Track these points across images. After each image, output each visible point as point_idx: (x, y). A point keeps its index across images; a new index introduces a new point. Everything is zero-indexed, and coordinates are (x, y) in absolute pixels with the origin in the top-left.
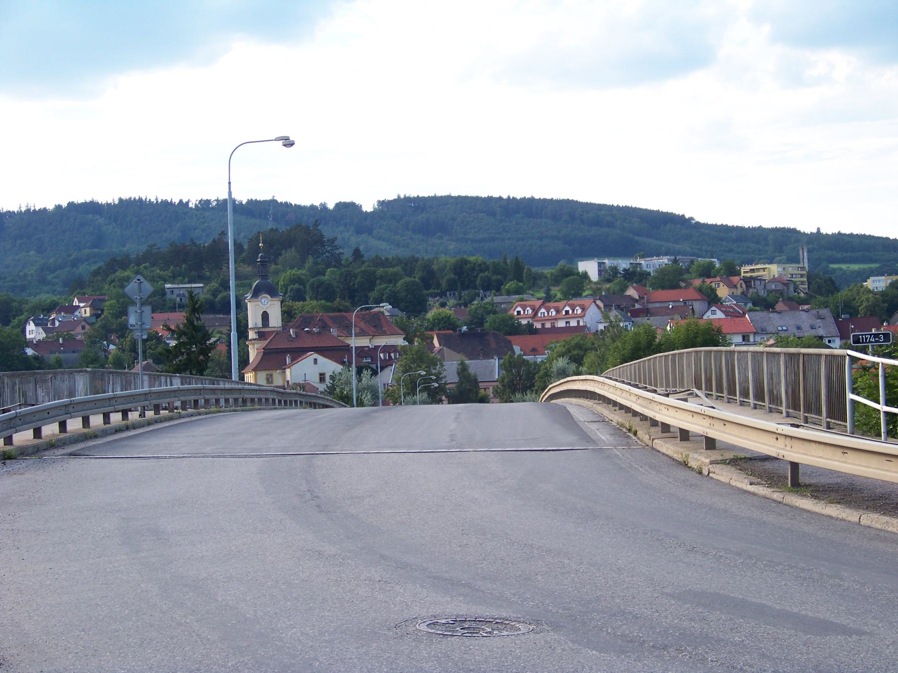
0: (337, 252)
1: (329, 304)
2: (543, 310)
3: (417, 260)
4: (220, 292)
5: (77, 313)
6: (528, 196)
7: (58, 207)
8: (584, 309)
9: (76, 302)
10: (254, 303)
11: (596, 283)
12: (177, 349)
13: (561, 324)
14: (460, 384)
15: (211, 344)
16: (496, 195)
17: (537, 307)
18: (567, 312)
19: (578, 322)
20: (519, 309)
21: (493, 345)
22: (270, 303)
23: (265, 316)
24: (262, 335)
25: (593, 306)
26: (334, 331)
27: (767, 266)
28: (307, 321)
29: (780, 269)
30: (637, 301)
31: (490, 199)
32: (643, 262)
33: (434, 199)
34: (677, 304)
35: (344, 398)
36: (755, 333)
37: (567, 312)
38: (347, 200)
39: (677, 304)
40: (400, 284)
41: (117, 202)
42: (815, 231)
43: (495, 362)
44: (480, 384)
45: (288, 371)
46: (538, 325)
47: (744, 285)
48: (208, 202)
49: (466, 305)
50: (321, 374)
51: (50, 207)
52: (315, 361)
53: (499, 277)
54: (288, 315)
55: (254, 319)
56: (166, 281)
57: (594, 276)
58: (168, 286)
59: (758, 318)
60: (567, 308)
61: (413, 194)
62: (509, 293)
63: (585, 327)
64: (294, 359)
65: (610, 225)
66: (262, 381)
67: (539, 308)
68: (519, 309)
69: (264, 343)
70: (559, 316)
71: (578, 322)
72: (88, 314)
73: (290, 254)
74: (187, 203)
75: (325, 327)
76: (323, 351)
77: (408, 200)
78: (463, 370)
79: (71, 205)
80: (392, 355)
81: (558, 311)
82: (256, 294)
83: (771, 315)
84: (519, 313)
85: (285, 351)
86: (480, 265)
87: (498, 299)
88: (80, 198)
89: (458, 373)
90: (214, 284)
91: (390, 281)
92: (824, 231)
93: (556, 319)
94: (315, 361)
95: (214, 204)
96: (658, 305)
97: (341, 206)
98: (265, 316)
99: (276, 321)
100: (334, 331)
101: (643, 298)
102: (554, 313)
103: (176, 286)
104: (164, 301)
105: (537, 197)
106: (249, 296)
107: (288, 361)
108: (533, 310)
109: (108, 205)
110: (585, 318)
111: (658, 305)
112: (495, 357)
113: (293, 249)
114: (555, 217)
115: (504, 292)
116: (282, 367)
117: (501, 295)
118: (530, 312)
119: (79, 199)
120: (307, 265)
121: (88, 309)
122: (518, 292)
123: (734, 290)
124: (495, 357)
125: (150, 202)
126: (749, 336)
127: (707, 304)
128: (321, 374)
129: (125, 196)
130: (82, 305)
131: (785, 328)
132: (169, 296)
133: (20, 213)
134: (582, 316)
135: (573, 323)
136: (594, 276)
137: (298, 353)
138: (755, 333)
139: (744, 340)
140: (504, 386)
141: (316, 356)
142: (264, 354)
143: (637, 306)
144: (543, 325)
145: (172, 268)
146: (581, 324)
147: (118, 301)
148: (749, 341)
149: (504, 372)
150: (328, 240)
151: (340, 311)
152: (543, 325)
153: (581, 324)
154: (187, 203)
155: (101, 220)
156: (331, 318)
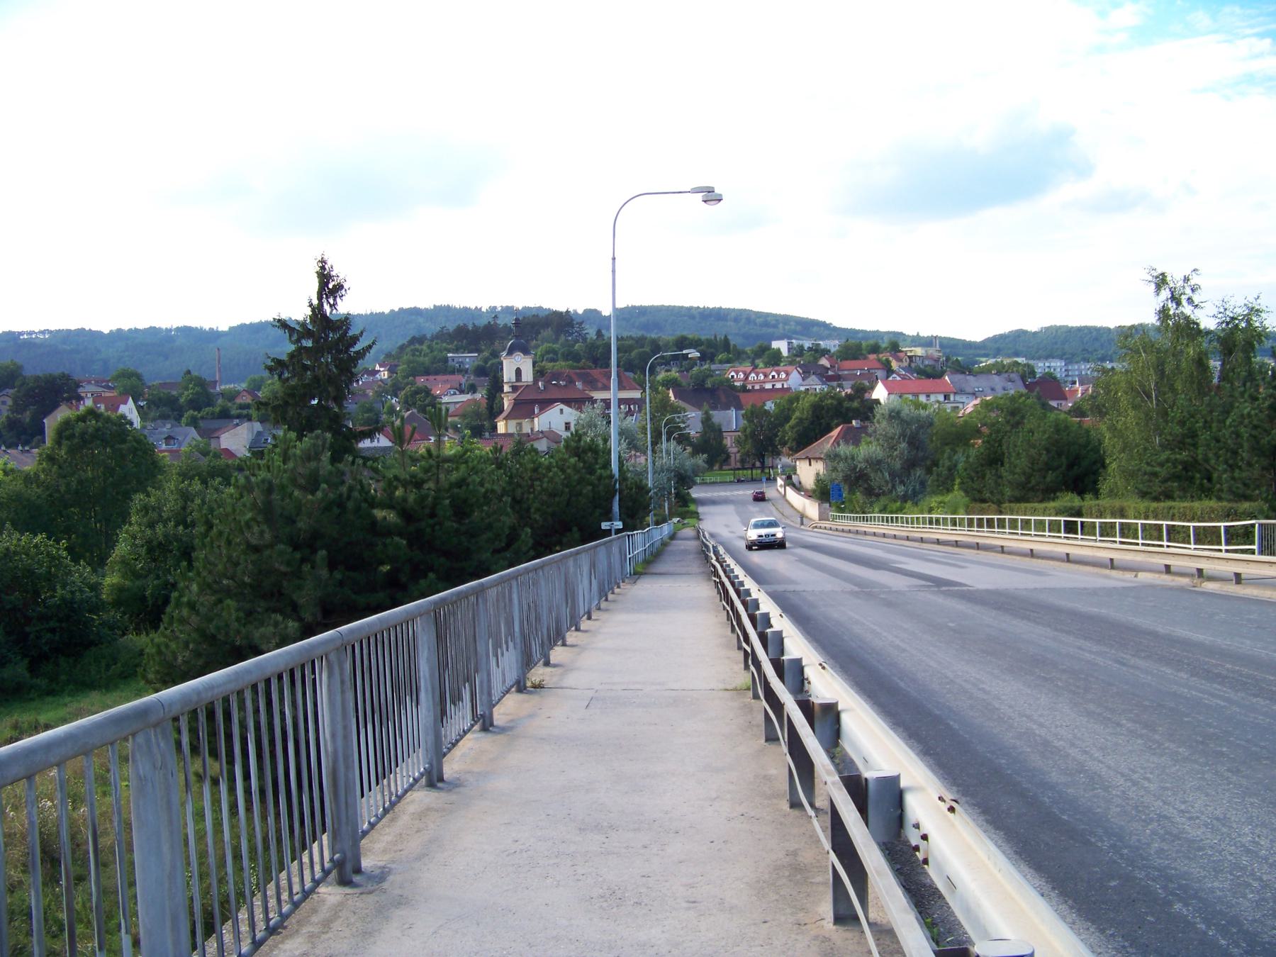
0: (584, 332)
1: (575, 364)
2: (753, 375)
3: (646, 339)
4: (491, 359)
5: (378, 376)
6: (718, 306)
7: (392, 311)
8: (788, 374)
9: (377, 368)
10: (509, 360)
11: (787, 357)
12: (295, 360)
13: (768, 386)
14: (704, 434)
15: (358, 353)
16: (695, 305)
17: (748, 372)
18: (773, 377)
19: (783, 385)
20: (733, 374)
21: (723, 399)
22: (523, 360)
23: (518, 372)
24: (515, 388)
25: (795, 372)
26: (579, 385)
27: (913, 349)
28: (557, 376)
29: (923, 352)
30: (828, 369)
31: (690, 309)
32: (821, 342)
33: (652, 307)
34: (863, 372)
35: (585, 452)
36: (955, 393)
37: (773, 377)
38: (592, 307)
39: (863, 372)
40: (633, 354)
41: (432, 307)
42: (915, 334)
43: (732, 413)
44: (724, 434)
45: (536, 420)
46: (749, 387)
47: (908, 360)
48: (495, 307)
49: (688, 371)
50: (566, 423)
51: (387, 311)
52: (562, 410)
53: (712, 350)
54: (539, 373)
55: (508, 374)
56: (449, 352)
57: (785, 352)
58: (450, 355)
59: (956, 380)
60: (774, 373)
61: (637, 304)
62: (721, 362)
63: (789, 389)
64: (542, 410)
65: (775, 326)
66: (512, 430)
67: (750, 373)
68: (733, 374)
69: (515, 395)
70: (766, 379)
71: (783, 385)
72: (386, 377)
73: (547, 333)
74: (481, 309)
75: (571, 382)
76: (567, 402)
77: (634, 307)
78: (707, 421)
79: (401, 309)
80: (632, 407)
81: (766, 376)
82: (510, 353)
83: (968, 377)
84: (733, 376)
85: (534, 402)
86: (696, 341)
87: (713, 367)
88: (407, 305)
89: (702, 422)
90: (486, 354)
91: (626, 352)
92: (921, 335)
93: (764, 382)
94: (562, 410)
95: (499, 309)
96: (846, 372)
97: (587, 312)
98: (518, 372)
99: (528, 376)
100: (579, 385)
101: (834, 367)
102: (762, 377)
103: (456, 355)
104: (446, 367)
105: (723, 307)
106: (504, 354)
107: (536, 411)
108: (745, 374)
109: (426, 309)
110: (789, 382)
111: (846, 372)
112: (732, 409)
113: (550, 329)
114: (736, 320)
115: (717, 362)
116: (531, 415)
117: (714, 364)
118: (742, 376)
119: (406, 306)
120: (560, 341)
121: (386, 373)
122: (728, 361)
123: (900, 364)
124: (732, 409)
125: (455, 308)
126: (949, 395)
127: (885, 372)
128: (566, 423)
129: (438, 304)
130: (382, 369)
131: (981, 389)
132: (450, 363)
133: (366, 315)
134: (786, 380)
135: (778, 386)
136: (785, 352)
137: (546, 404)
138: (955, 393)
139: (945, 399)
140: (746, 436)
141: (562, 406)
142: (515, 404)
143: (830, 373)
144: (753, 387)
145: (455, 342)
146: (785, 386)
147: (408, 366)
148: (949, 399)
149: (745, 422)
150: (577, 323)
151: (584, 369)
152: (753, 387)
153: (785, 386)
154: (481, 309)
155: (421, 320)
156: (576, 374)
